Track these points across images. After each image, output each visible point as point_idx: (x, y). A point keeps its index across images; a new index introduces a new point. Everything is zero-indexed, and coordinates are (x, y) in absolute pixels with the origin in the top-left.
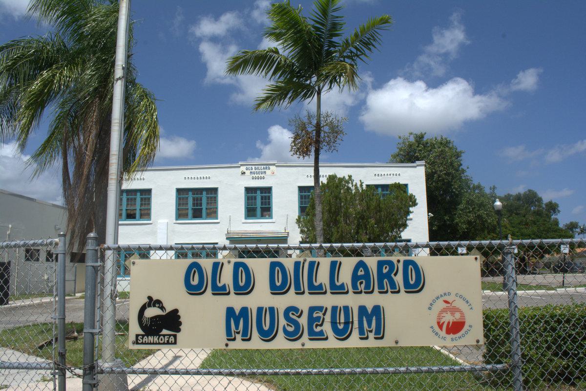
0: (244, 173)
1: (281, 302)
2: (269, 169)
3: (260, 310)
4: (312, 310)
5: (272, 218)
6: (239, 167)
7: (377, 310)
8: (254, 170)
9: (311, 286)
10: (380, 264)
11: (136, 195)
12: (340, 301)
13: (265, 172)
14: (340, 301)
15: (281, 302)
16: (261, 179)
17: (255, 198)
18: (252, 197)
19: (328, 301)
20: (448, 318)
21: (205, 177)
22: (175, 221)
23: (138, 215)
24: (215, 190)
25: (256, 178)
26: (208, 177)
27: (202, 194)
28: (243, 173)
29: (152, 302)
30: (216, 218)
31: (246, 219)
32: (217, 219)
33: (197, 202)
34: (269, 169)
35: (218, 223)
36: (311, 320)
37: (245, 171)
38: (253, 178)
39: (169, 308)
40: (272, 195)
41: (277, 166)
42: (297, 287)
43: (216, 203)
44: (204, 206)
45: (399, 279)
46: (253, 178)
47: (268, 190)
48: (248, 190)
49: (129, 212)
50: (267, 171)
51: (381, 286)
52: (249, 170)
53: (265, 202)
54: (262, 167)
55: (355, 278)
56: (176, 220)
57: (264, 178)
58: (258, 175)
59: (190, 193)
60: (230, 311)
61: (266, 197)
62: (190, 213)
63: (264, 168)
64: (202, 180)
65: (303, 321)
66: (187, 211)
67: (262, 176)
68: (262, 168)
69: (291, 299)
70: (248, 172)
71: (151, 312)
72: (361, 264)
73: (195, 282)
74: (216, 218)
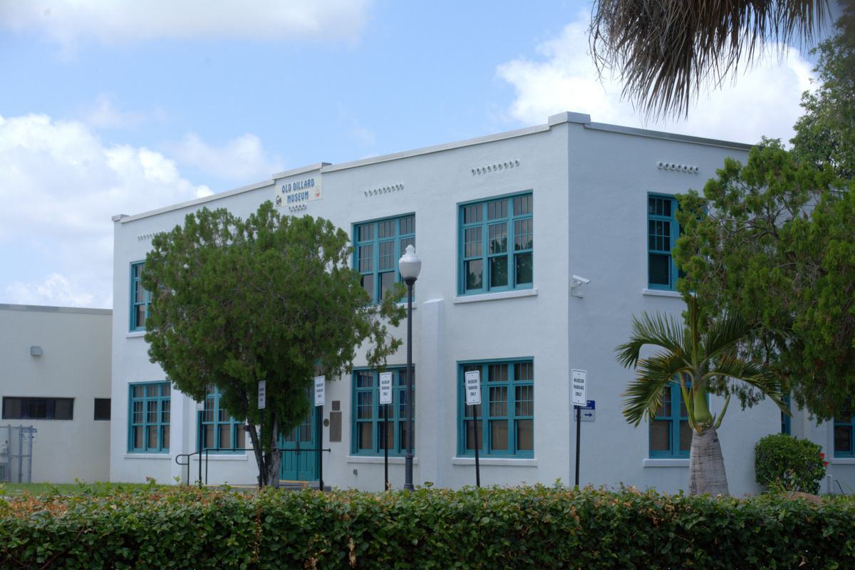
1: (295, 193)
56: (461, 292)
64: (498, 171)
68: (303, 186)
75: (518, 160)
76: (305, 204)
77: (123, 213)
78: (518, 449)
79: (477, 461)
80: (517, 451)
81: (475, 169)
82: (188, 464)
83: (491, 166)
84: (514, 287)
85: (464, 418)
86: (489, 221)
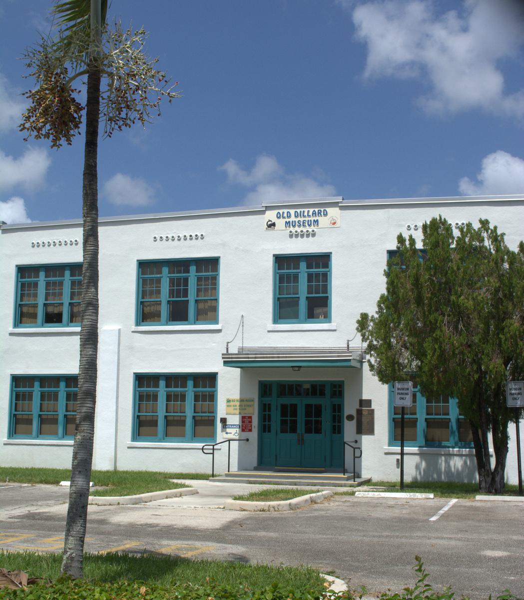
0: (274, 224)
1: (297, 220)
2: (326, 215)
3: (292, 221)
4: (303, 221)
5: (330, 322)
6: (262, 212)
7: (317, 220)
8: (293, 218)
9: (303, 216)
10: (318, 210)
11: (63, 276)
12: (309, 219)
13: (316, 222)
14: (309, 219)
15: (297, 220)
16: (308, 236)
17: (296, 277)
18: (289, 276)
19: (307, 219)
20: (333, 222)
21: (188, 236)
22: (134, 328)
23: (65, 317)
24: (213, 263)
25: (297, 236)
26: (199, 235)
27: (188, 272)
28: (272, 225)
29: (269, 221)
30: (215, 320)
31: (275, 321)
32: (217, 323)
33: (179, 287)
34: (326, 215)
35: (219, 331)
36: (303, 223)
37: (274, 219)
38: (291, 236)
39: (273, 222)
40: (330, 271)
41: (342, 208)
42: (300, 216)
43: (215, 289)
44: (192, 297)
45: (322, 214)
46: (291, 236)
47: (322, 260)
48: (281, 261)
49: (50, 309)
50: (321, 219)
51: (318, 215)
52: (284, 218)
53: (317, 286)
54: (311, 210)
55: (313, 214)
57: (314, 235)
58: (302, 228)
59: (165, 270)
60: (286, 222)
61: (317, 275)
62: (164, 310)
63: (314, 213)
64: (188, 241)
65: (302, 223)
66: (158, 307)
67: (310, 230)
68: (311, 214)
69: (299, 219)
70: (280, 223)
71: (269, 223)
72: (314, 211)
73: (279, 216)
74: (215, 320)
75: (204, 234)
76: (315, 230)
77: (5, 221)
78: (15, 433)
79: (402, 450)
80: (193, 438)
81: (35, 242)
82: (355, 458)
83: (176, 236)
84: (306, 321)
85: (137, 414)
86: (170, 275)
